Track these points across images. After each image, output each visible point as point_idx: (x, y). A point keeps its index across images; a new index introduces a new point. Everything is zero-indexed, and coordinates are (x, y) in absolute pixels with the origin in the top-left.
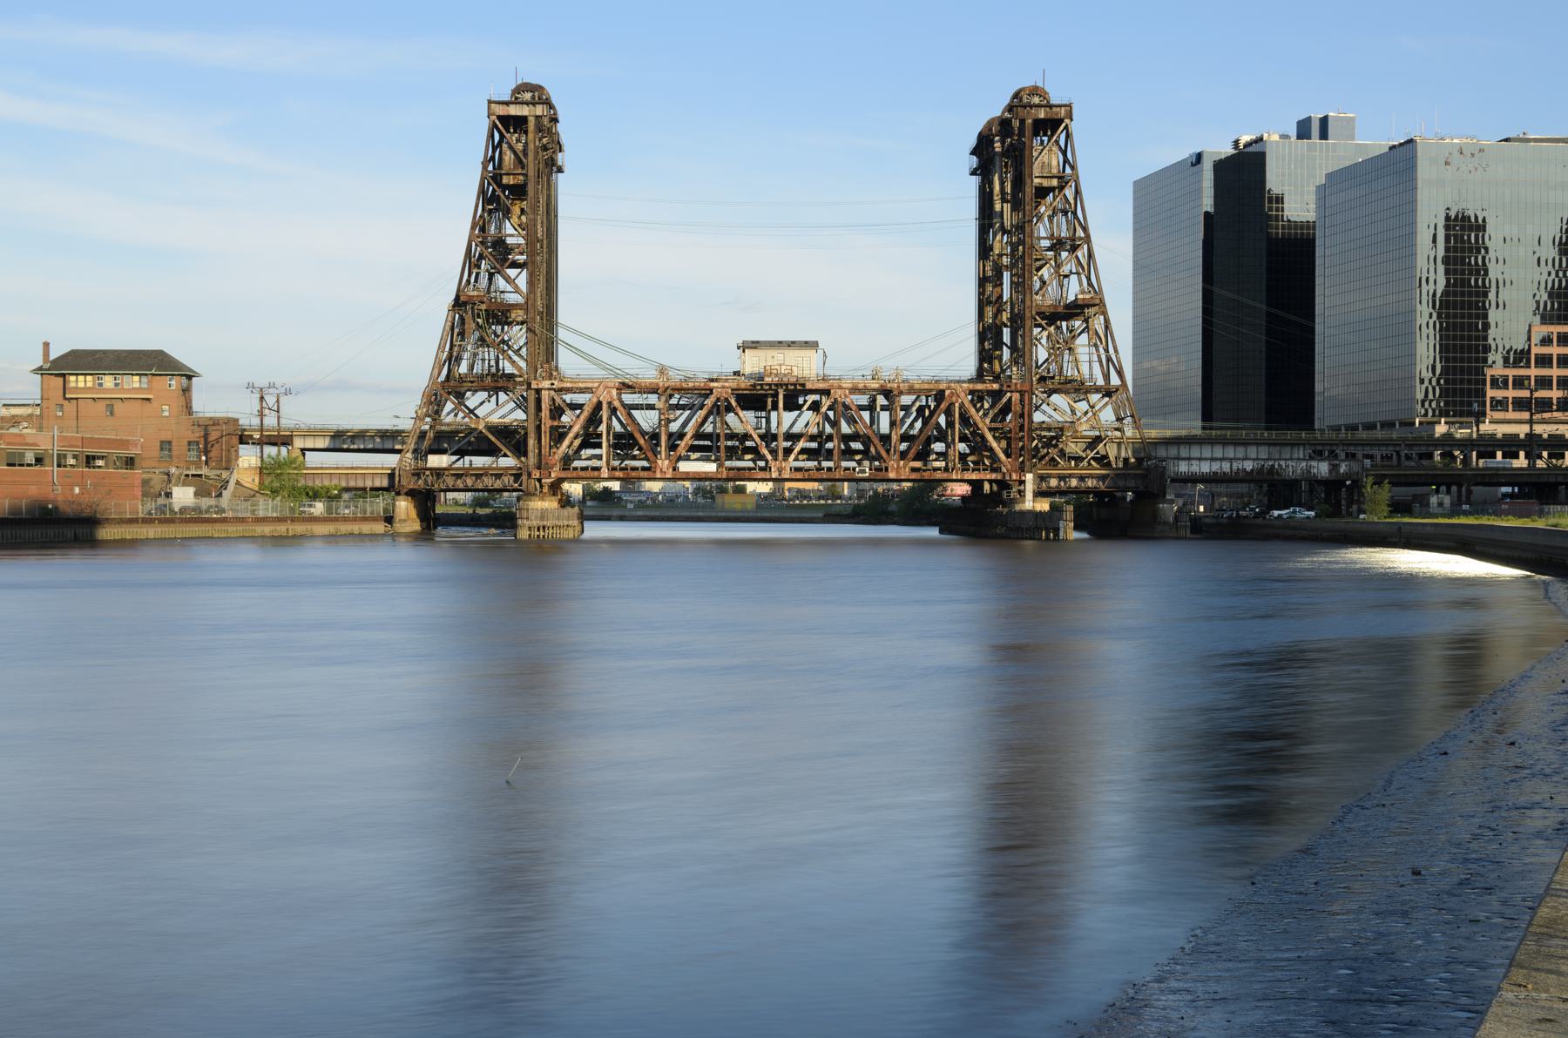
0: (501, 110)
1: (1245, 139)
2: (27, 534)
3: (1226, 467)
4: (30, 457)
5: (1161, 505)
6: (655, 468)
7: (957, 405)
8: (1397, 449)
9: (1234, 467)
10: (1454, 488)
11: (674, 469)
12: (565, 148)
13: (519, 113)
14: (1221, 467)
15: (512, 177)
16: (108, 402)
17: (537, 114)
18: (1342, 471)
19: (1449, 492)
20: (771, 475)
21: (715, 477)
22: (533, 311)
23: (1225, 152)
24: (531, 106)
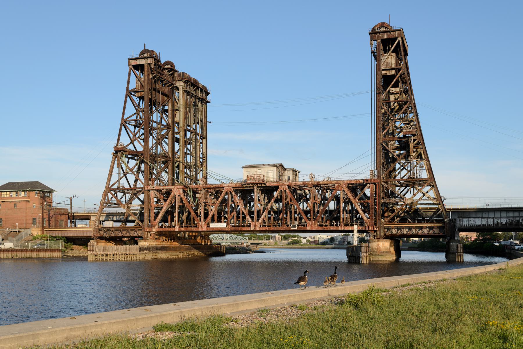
0: (133, 63)
5: (451, 243)
6: (198, 226)
9: (496, 222)
13: (141, 63)
14: (488, 221)
15: (139, 93)
16: (15, 203)
17: (149, 63)
21: (225, 230)
22: (146, 154)
24: (146, 59)
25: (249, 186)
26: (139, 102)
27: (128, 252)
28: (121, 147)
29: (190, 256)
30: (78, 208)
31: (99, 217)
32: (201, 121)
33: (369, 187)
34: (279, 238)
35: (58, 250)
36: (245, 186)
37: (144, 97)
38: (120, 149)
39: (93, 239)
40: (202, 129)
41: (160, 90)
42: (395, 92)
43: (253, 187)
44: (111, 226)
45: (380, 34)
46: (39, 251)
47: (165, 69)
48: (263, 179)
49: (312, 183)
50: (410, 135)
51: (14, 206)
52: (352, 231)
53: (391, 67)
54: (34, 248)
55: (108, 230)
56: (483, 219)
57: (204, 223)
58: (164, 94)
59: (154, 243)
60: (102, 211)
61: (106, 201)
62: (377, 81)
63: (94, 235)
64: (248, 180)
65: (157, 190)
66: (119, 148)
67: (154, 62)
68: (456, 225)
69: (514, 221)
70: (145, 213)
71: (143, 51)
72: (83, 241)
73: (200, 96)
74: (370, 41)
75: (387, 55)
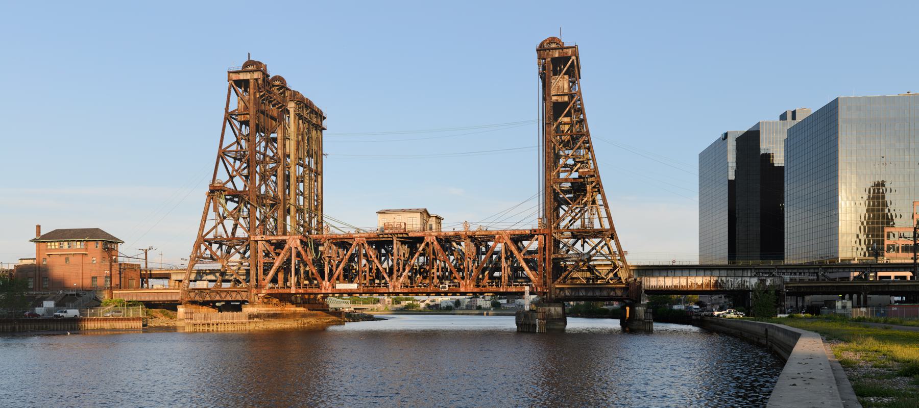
0: (235, 77)
2: (56, 327)
5: (637, 308)
6: (321, 287)
8: (816, 271)
9: (689, 282)
10: (855, 296)
11: (333, 287)
13: (245, 78)
15: (242, 116)
16: (66, 256)
18: (768, 284)
19: (851, 298)
20: (389, 290)
23: (740, 132)
24: (251, 73)
25: (387, 236)
26: (241, 127)
27: (235, 321)
28: (218, 185)
29: (306, 325)
30: (155, 263)
31: (188, 275)
32: (315, 152)
33: (537, 239)
34: (388, 301)
35: (138, 319)
36: (381, 236)
37: (249, 121)
38: (217, 188)
39: (181, 304)
40: (316, 163)
41: (268, 112)
42: (563, 123)
43: (392, 238)
44: (205, 287)
45: (550, 51)
46: (113, 320)
47: (274, 86)
48: (405, 229)
49: (466, 234)
50: (587, 176)
51: (65, 261)
52: (523, 293)
53: (563, 92)
54: (106, 316)
55: (201, 292)
56: (674, 280)
57: (328, 283)
58: (273, 118)
59: (264, 309)
60: (192, 268)
61: (199, 254)
62: (547, 110)
63: (182, 299)
64: (385, 229)
65: (266, 241)
66: (216, 187)
67: (262, 77)
69: (712, 281)
70: (251, 271)
71: (247, 62)
72: (172, 306)
73: (314, 122)
74: (537, 60)
75: (559, 78)
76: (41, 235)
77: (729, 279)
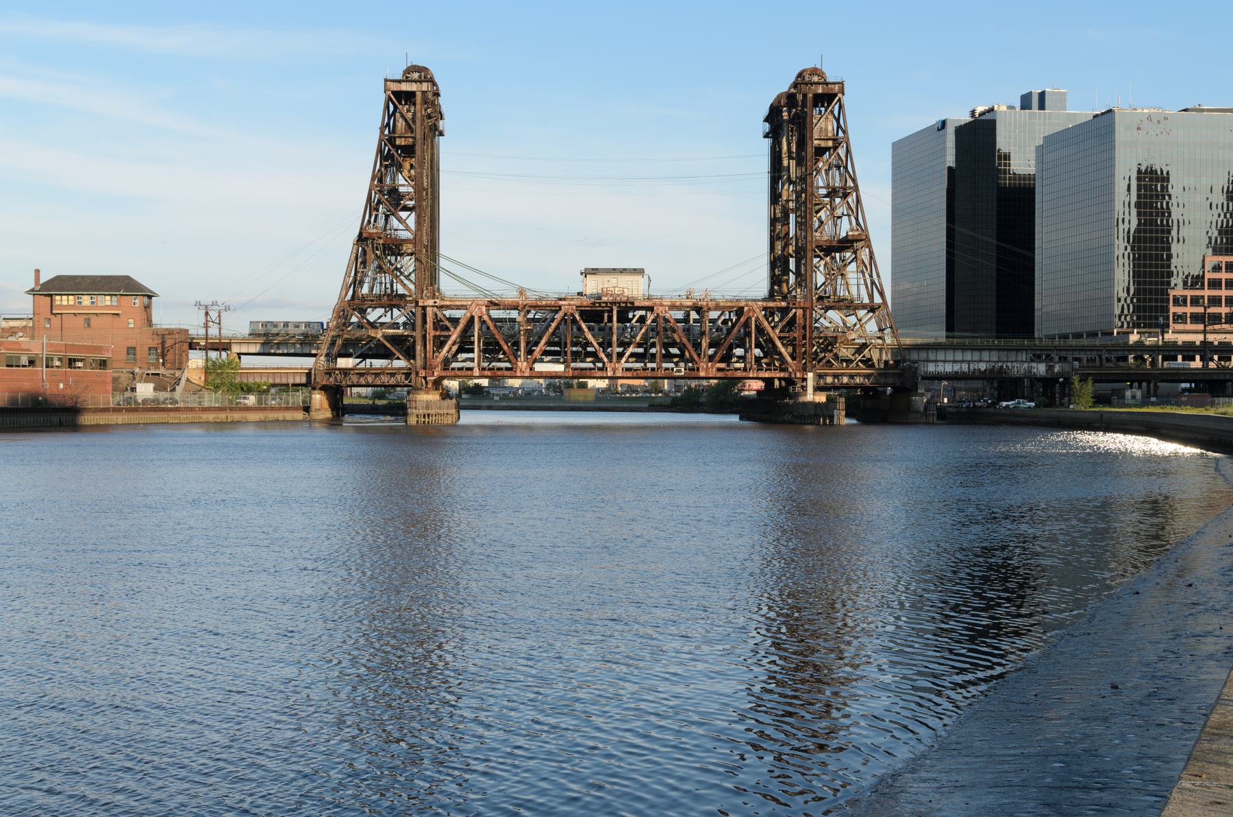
0: (395, 87)
1: (980, 109)
3: (965, 367)
4: (24, 360)
7: (753, 319)
9: (972, 368)
10: (1144, 384)
11: (531, 369)
12: (445, 116)
13: (409, 89)
16: (86, 317)
18: (1056, 371)
19: (1140, 387)
68: (919, 372)
76: (41, 282)
77: (1015, 364)
